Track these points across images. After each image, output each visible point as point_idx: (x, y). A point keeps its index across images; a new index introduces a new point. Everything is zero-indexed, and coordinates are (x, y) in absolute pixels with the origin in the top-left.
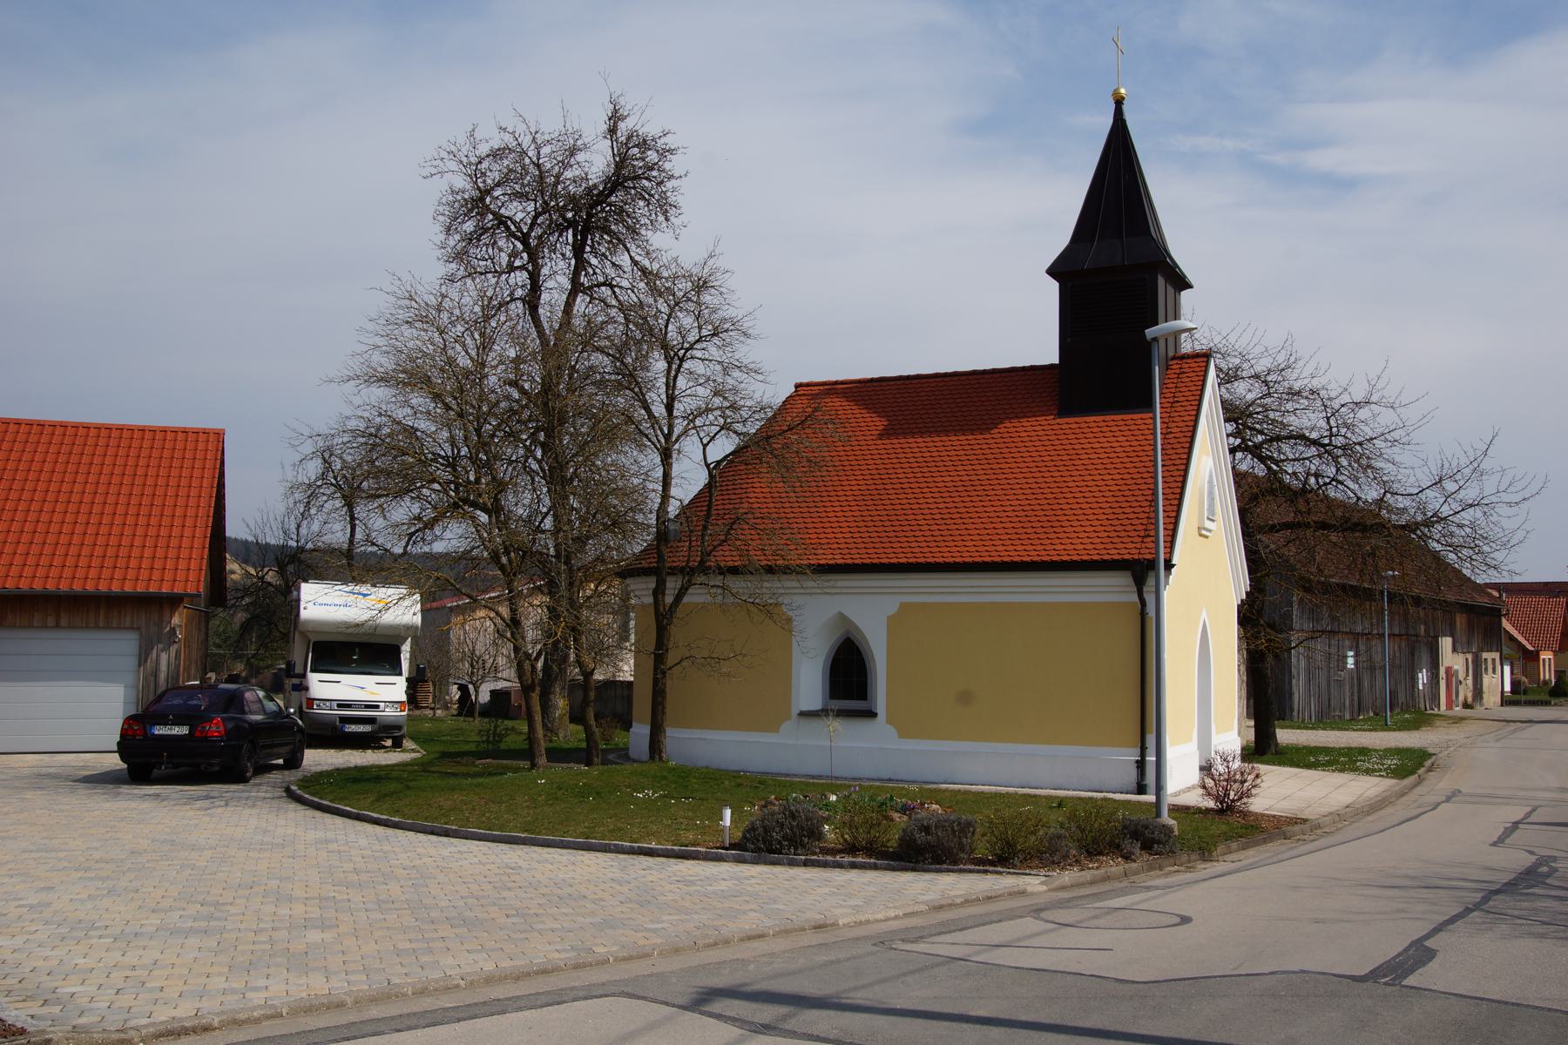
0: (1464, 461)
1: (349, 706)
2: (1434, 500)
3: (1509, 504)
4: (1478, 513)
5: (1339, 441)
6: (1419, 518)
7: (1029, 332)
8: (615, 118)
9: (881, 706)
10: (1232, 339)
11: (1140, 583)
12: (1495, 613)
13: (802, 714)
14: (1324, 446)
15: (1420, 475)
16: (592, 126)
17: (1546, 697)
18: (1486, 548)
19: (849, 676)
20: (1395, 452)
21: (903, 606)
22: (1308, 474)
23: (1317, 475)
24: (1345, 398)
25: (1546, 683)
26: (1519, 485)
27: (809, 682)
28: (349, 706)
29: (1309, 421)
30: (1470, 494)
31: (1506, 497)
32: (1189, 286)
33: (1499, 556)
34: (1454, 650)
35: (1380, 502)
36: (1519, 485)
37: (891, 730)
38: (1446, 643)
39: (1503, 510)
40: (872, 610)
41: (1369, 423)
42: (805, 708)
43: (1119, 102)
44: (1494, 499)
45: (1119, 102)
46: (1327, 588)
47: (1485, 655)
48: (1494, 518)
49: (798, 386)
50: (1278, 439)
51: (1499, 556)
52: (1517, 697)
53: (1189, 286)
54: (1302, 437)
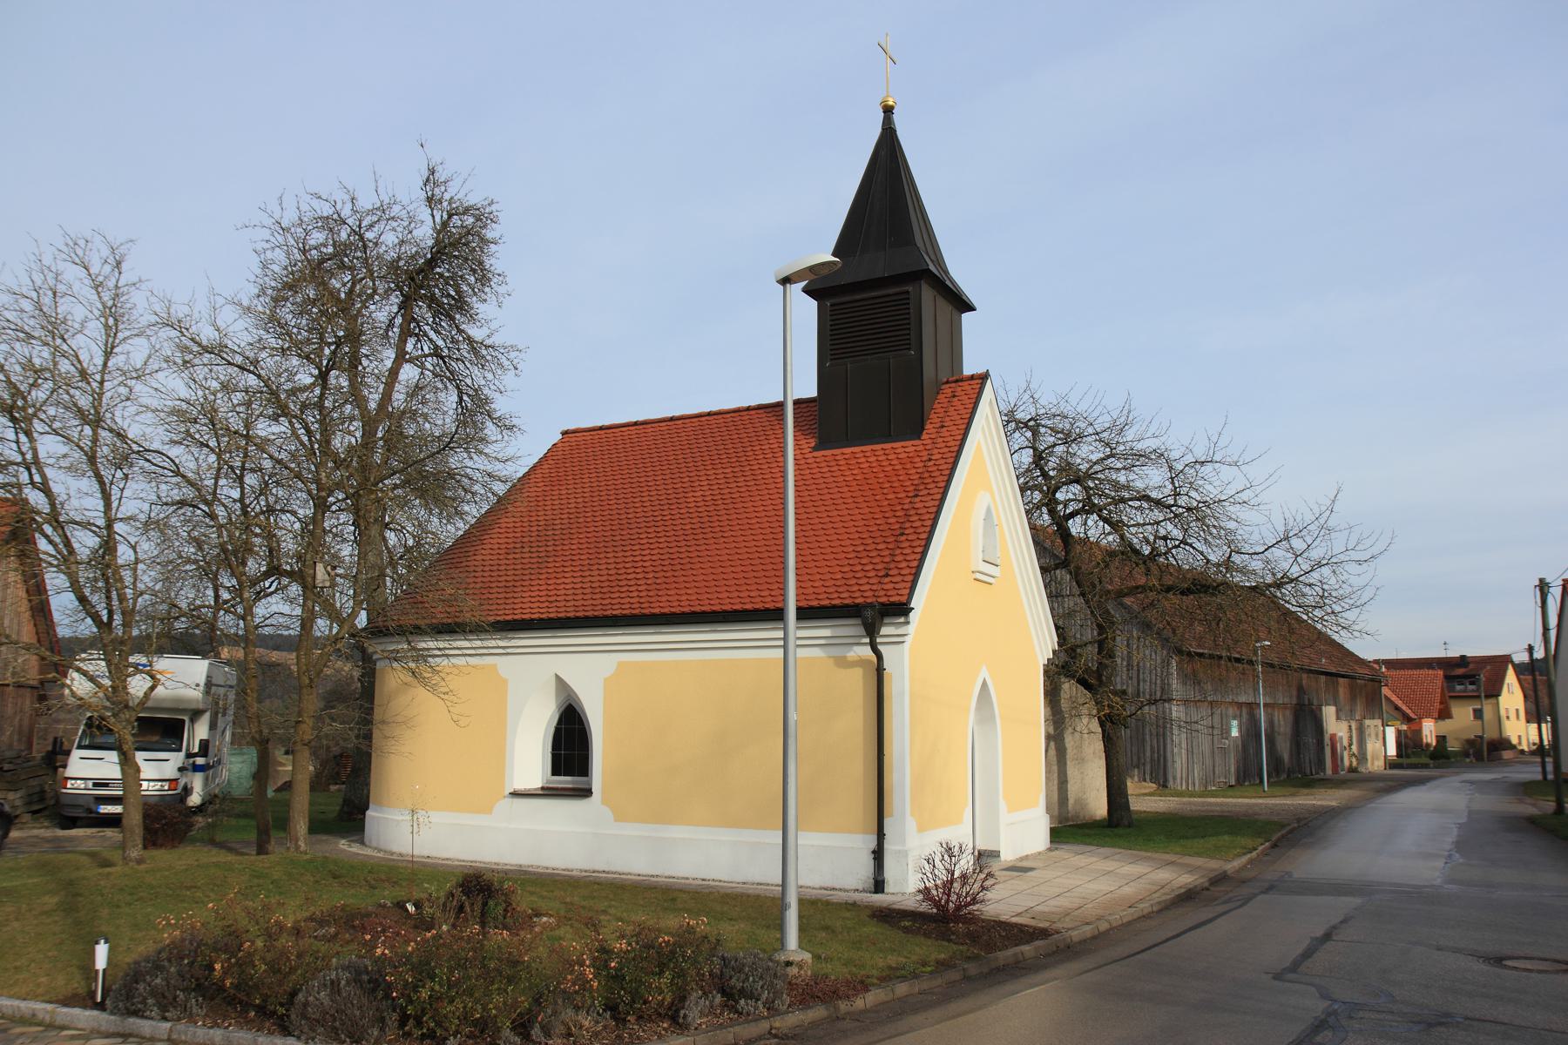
0: (1309, 517)
1: (106, 785)
2: (1282, 561)
3: (1359, 562)
4: (1326, 571)
5: (1182, 501)
6: (1269, 580)
7: (774, 356)
8: (431, 179)
9: (597, 785)
10: (1073, 400)
11: (872, 631)
12: (1376, 681)
13: (516, 794)
14: (1169, 507)
15: (1266, 533)
16: (410, 193)
17: (1425, 760)
18: (1337, 608)
19: (571, 745)
20: (1243, 514)
21: (620, 664)
22: (1156, 537)
23: (1165, 538)
24: (1189, 458)
25: (1428, 745)
26: (1368, 543)
27: (530, 760)
28: (106, 785)
29: (1153, 479)
30: (1315, 554)
31: (1355, 555)
32: (972, 309)
33: (1351, 615)
34: (1338, 718)
35: (1228, 563)
36: (1368, 543)
37: (607, 813)
38: (1329, 712)
39: (1353, 568)
40: (595, 668)
41: (1215, 483)
42: (520, 786)
43: (888, 111)
44: (1342, 557)
45: (888, 111)
46: (1189, 654)
47: (1367, 722)
48: (1345, 577)
49: (564, 433)
50: (1123, 500)
51: (1351, 615)
52: (1404, 761)
53: (972, 309)
54: (1147, 498)
